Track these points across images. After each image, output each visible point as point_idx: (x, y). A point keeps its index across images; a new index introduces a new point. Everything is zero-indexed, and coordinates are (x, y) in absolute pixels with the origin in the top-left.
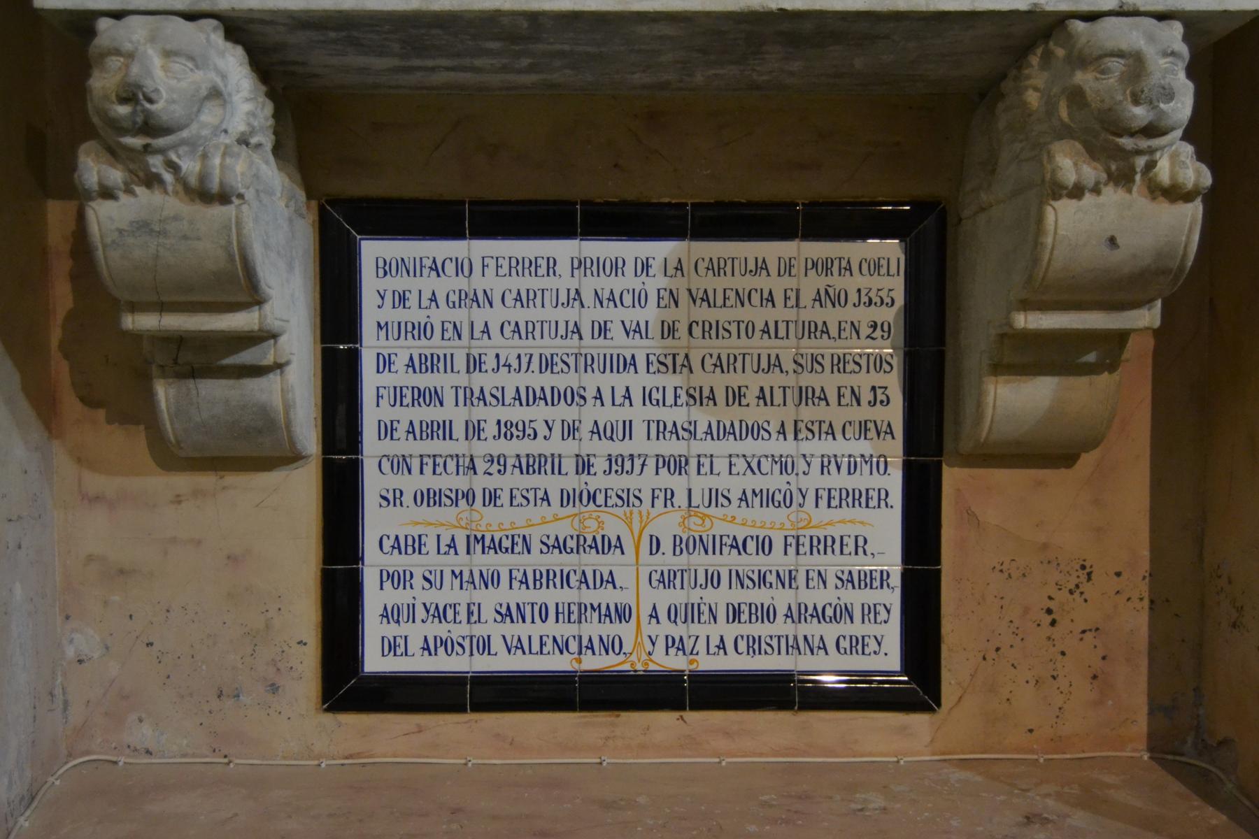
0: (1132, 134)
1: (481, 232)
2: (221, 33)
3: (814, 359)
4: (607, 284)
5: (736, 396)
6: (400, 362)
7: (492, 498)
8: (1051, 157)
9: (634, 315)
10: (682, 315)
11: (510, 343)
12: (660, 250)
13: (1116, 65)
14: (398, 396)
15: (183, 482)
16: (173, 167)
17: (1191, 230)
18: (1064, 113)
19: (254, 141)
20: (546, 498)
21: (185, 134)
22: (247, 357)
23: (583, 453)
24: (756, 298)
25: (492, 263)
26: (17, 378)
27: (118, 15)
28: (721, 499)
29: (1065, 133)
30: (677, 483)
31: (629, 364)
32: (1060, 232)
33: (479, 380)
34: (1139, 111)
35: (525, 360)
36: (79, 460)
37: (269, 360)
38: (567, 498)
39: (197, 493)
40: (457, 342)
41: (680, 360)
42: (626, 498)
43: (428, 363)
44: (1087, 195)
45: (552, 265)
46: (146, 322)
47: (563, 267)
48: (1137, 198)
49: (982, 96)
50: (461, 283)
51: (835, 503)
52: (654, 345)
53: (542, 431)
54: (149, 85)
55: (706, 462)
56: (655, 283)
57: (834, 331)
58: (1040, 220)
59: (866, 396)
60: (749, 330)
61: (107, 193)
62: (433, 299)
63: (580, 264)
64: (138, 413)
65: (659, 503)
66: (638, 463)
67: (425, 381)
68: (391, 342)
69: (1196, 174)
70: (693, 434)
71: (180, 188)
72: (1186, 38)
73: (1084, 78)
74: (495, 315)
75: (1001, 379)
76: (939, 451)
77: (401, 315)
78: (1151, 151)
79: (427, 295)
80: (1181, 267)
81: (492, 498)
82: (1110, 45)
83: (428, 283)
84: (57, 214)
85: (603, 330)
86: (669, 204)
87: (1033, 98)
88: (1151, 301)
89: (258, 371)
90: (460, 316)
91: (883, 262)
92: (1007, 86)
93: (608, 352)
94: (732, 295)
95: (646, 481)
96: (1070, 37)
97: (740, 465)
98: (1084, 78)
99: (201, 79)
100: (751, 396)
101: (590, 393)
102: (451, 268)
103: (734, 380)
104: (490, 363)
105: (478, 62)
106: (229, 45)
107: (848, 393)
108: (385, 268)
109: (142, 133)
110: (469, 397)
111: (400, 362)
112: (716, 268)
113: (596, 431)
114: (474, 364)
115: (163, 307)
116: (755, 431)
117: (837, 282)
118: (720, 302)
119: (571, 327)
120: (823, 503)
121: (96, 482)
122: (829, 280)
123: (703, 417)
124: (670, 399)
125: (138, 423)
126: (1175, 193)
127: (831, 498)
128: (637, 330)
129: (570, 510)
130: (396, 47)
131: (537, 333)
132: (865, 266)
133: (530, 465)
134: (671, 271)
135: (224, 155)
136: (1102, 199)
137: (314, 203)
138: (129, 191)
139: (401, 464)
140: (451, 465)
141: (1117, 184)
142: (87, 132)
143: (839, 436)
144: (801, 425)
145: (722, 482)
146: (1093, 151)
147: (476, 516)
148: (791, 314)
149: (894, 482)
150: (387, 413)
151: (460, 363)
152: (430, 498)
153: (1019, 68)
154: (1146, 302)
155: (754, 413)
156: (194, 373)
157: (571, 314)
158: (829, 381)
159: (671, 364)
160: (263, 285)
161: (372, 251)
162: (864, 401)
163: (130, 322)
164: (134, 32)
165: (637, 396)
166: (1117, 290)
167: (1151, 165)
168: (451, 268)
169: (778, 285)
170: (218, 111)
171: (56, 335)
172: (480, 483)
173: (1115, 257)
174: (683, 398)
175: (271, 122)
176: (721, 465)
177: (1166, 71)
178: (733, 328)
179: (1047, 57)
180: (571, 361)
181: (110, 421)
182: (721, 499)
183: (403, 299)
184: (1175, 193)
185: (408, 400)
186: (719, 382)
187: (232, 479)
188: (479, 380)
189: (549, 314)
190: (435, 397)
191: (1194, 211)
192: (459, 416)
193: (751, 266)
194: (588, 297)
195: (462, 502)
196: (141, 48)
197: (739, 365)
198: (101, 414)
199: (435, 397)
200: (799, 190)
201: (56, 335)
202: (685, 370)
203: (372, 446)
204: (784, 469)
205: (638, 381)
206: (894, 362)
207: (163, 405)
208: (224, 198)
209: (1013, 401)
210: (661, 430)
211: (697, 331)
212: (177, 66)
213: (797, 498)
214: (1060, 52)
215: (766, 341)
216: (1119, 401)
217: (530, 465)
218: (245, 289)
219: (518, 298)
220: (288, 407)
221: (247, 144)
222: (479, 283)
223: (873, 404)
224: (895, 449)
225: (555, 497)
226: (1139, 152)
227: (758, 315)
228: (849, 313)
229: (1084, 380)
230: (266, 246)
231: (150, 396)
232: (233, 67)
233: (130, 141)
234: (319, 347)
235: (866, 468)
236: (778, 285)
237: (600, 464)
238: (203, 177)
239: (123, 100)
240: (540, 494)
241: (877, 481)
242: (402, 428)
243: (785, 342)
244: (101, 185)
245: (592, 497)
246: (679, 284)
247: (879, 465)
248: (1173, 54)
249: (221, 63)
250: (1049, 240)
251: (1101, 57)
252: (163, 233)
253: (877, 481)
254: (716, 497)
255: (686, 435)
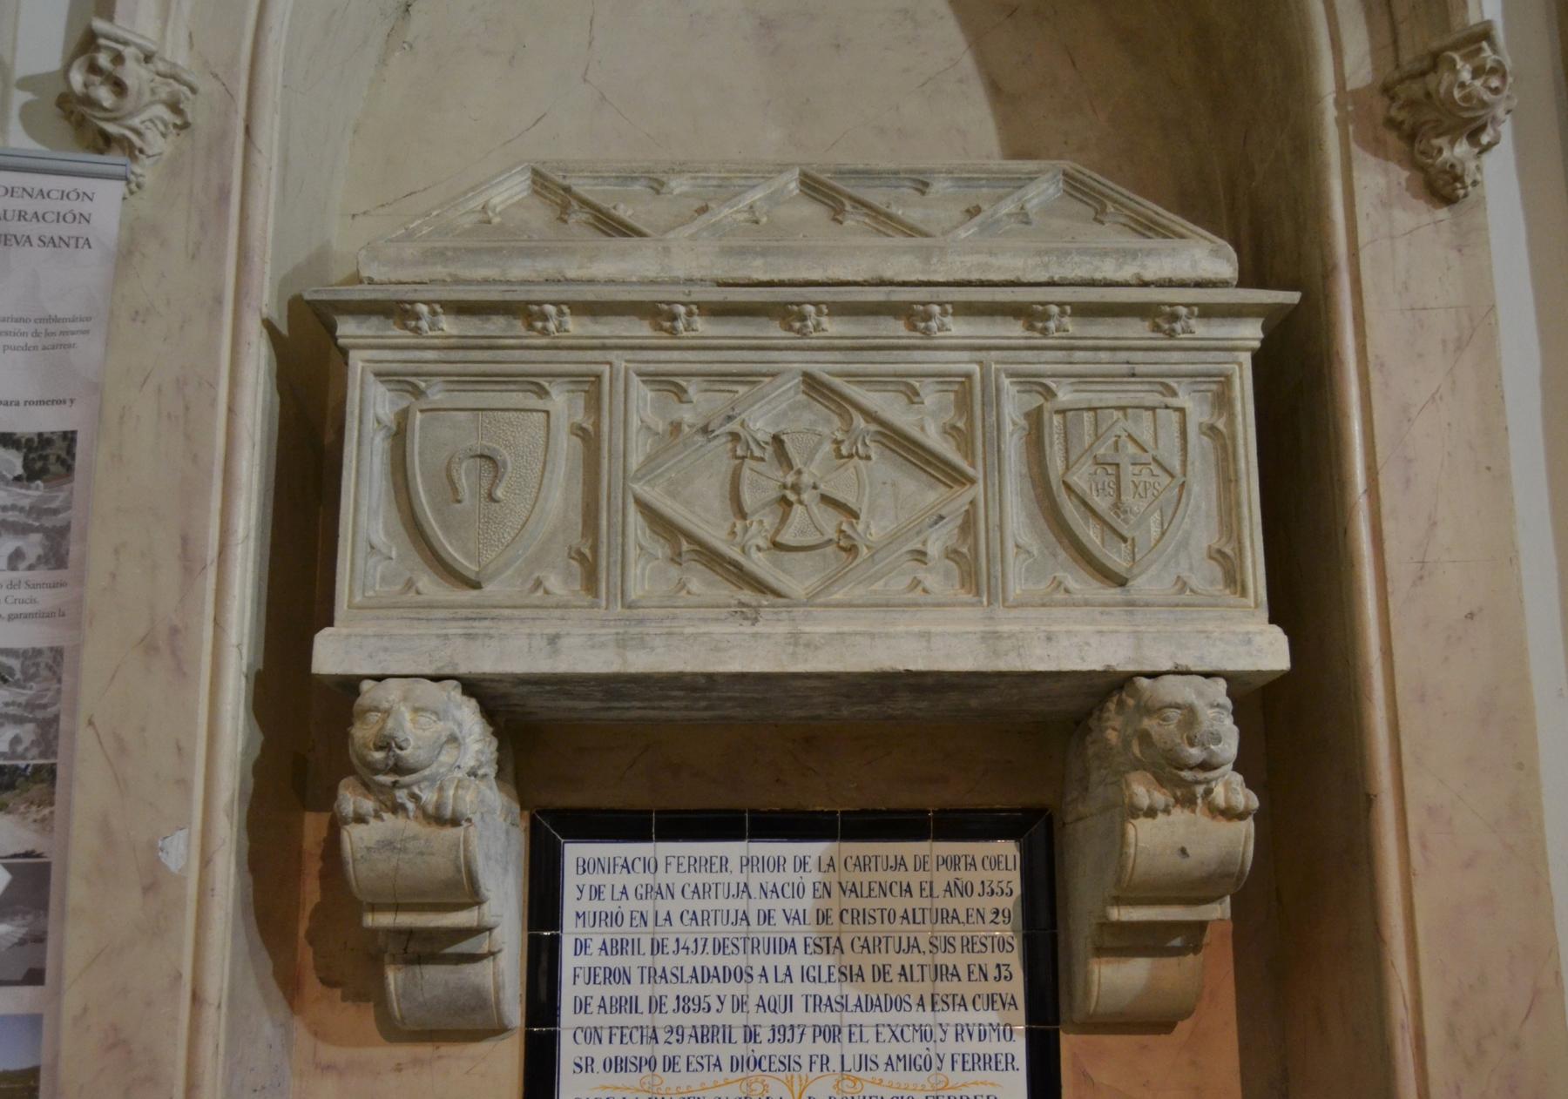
0: (1191, 769)
1: (664, 836)
2: (459, 690)
3: (947, 941)
4: (770, 878)
5: (881, 973)
6: (595, 946)
7: (671, 1064)
8: (1128, 786)
9: (792, 905)
10: (834, 904)
11: (688, 929)
12: (815, 850)
13: (1174, 714)
14: (592, 976)
15: (403, 1052)
16: (415, 798)
17: (1246, 842)
18: (1136, 750)
19: (481, 772)
20: (718, 1064)
21: (427, 772)
22: (465, 947)
23: (751, 1024)
24: (896, 889)
25: (674, 862)
26: (270, 964)
27: (379, 678)
28: (870, 1064)
29: (1138, 765)
30: (833, 1050)
31: (790, 946)
32: (1141, 844)
33: (661, 961)
34: (1194, 751)
35: (701, 944)
36: (316, 1034)
37: (485, 949)
38: (736, 1064)
39: (417, 1062)
40: (643, 928)
41: (833, 943)
42: (788, 1064)
43: (619, 947)
44: (1160, 815)
45: (724, 863)
46: (385, 920)
47: (734, 864)
48: (1201, 818)
49: (1077, 723)
50: (648, 878)
51: (969, 1066)
52: (810, 930)
53: (715, 1005)
54: (400, 736)
55: (856, 1030)
56: (811, 877)
57: (963, 918)
58: (1123, 834)
59: (992, 972)
60: (891, 916)
61: (360, 819)
62: (624, 892)
63: (748, 862)
64: (370, 992)
65: (816, 1067)
66: (798, 1032)
67: (615, 962)
68: (588, 929)
69: (1245, 798)
70: (845, 1007)
71: (420, 814)
72: (1229, 694)
73: (1148, 723)
74: (675, 906)
75: (1104, 959)
76: (1057, 1022)
77: (597, 906)
78: (1208, 782)
79: (618, 889)
80: (1242, 872)
81: (671, 1064)
82: (1168, 699)
83: (621, 879)
84: (313, 827)
85: (767, 917)
86: (822, 812)
87: (1112, 736)
88: (1221, 897)
89: (474, 958)
90: (647, 906)
91: (1002, 859)
92: (1092, 723)
93: (772, 936)
94: (876, 887)
95: (805, 1048)
96: (1136, 693)
97: (886, 1033)
98: (1148, 723)
99: (443, 728)
100: (894, 972)
101: (756, 972)
102: (639, 866)
103: (879, 959)
104: (671, 946)
105: (664, 704)
106: (465, 698)
107: (976, 970)
108: (584, 866)
109: (391, 773)
110: (653, 975)
111: (595, 946)
112: (862, 865)
113: (762, 1005)
114: (658, 947)
115: (398, 908)
116: (897, 1004)
117: (965, 876)
118: (866, 893)
119: (742, 887)
120: (958, 1066)
121: (329, 1053)
122: (958, 874)
123: (852, 991)
124: (825, 977)
125: (368, 1000)
126: (1230, 814)
127: (966, 1063)
128: (795, 917)
129: (739, 1074)
130: (599, 695)
131: (712, 920)
132: (987, 862)
133: (705, 1035)
134: (824, 867)
135: (457, 788)
136: (1171, 818)
137: (526, 813)
138: (377, 816)
139: (593, 1035)
140: (636, 1035)
141: (1183, 806)
142: (350, 770)
143: (970, 1007)
144: (937, 998)
145: (870, 1049)
146: (1161, 781)
147: (657, 1081)
148: (926, 903)
149: (1018, 1048)
150: (583, 932)
151: (646, 946)
152: (618, 1065)
153: (1101, 710)
154: (1217, 898)
155: (897, 988)
156: (420, 960)
157: (741, 904)
158: (959, 960)
159: (826, 946)
160: (483, 890)
161: (573, 852)
162: (990, 977)
163: (370, 920)
164: (391, 693)
165: (796, 974)
166: (1196, 890)
167: (1208, 792)
168: (639, 866)
169: (914, 878)
170: (455, 752)
171: (303, 926)
172: (661, 1051)
173: (1185, 864)
174: (836, 975)
175: (495, 755)
176: (869, 1034)
177: (1214, 719)
178: (878, 915)
179: (1121, 704)
180: (740, 944)
181: (344, 998)
182: (870, 1064)
183: (598, 892)
184: (1230, 814)
185: (600, 979)
186: (867, 961)
187: (447, 1049)
188: (661, 961)
189: (722, 904)
190: (624, 976)
191: (1247, 827)
192: (643, 992)
193: (892, 863)
194: (755, 890)
195: (645, 1069)
196: (396, 706)
197: (883, 946)
198: (338, 992)
199: (624, 976)
200: (930, 799)
201: (303, 926)
202: (838, 951)
203: (568, 1018)
204: (923, 1037)
205: (797, 961)
206: (1015, 943)
207: (392, 987)
208: (455, 822)
209: (1116, 979)
210: (817, 1003)
211: (847, 917)
212: (423, 719)
213: (936, 1063)
214: (1131, 702)
215: (905, 926)
216: (1209, 977)
217: (705, 1035)
218: (467, 891)
219: (696, 891)
220: (498, 988)
221: (476, 776)
222: (662, 878)
223: (998, 979)
224: (1018, 1021)
225: (726, 1064)
226: (1198, 782)
227: (899, 904)
228: (975, 902)
229: (1174, 960)
230: (488, 857)
231: (382, 978)
232: (468, 716)
233: (382, 778)
234: (526, 934)
235: (995, 1035)
236: (914, 878)
237: (765, 1034)
238: (439, 806)
239: (379, 748)
240: (713, 1061)
241: (1003, 1047)
242: (595, 1003)
243: (922, 927)
244: (355, 812)
245: (758, 1063)
246: (831, 878)
247: (1006, 1032)
248: (1218, 706)
249: (458, 714)
250: (1132, 851)
251: (1160, 709)
252: (404, 850)
253: (1003, 1047)
254: (865, 1062)
255: (839, 1007)
